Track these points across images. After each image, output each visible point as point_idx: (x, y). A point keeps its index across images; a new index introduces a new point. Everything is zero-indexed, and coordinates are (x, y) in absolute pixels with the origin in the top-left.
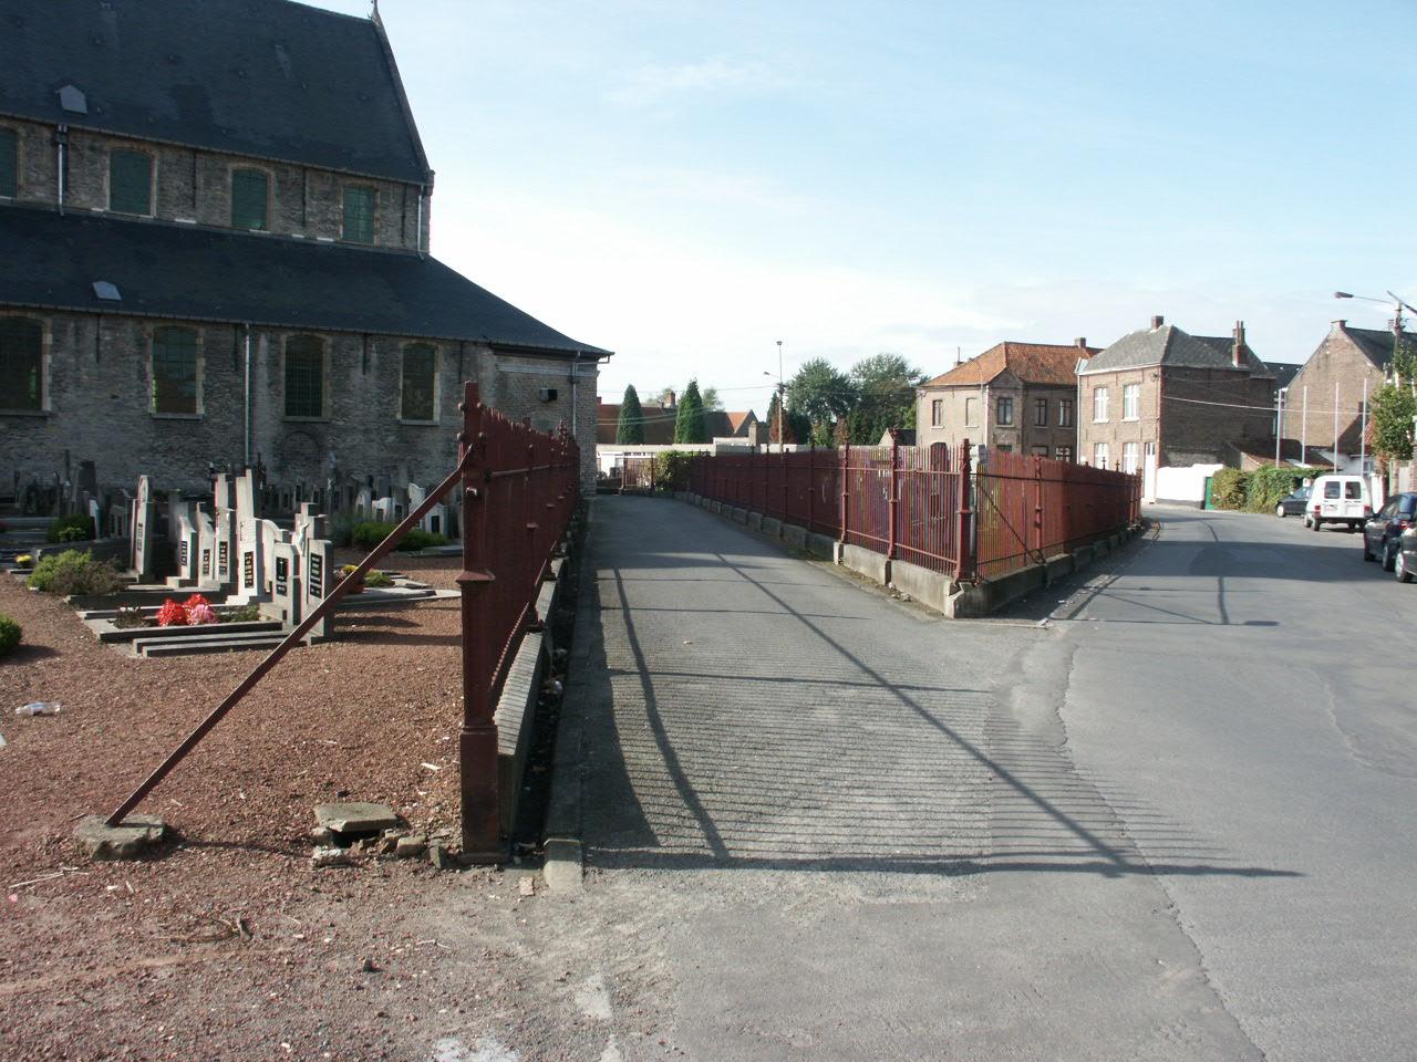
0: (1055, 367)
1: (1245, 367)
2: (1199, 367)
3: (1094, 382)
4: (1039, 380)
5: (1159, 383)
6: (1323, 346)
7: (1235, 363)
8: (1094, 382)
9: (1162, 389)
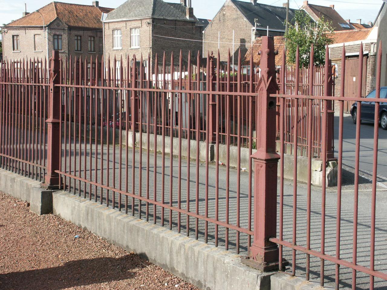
0: (84, 17)
1: (192, 19)
2: (171, 19)
3: (112, 26)
4: (76, 25)
5: (151, 27)
6: (222, 9)
7: (188, 17)
8: (112, 26)
9: (152, 31)
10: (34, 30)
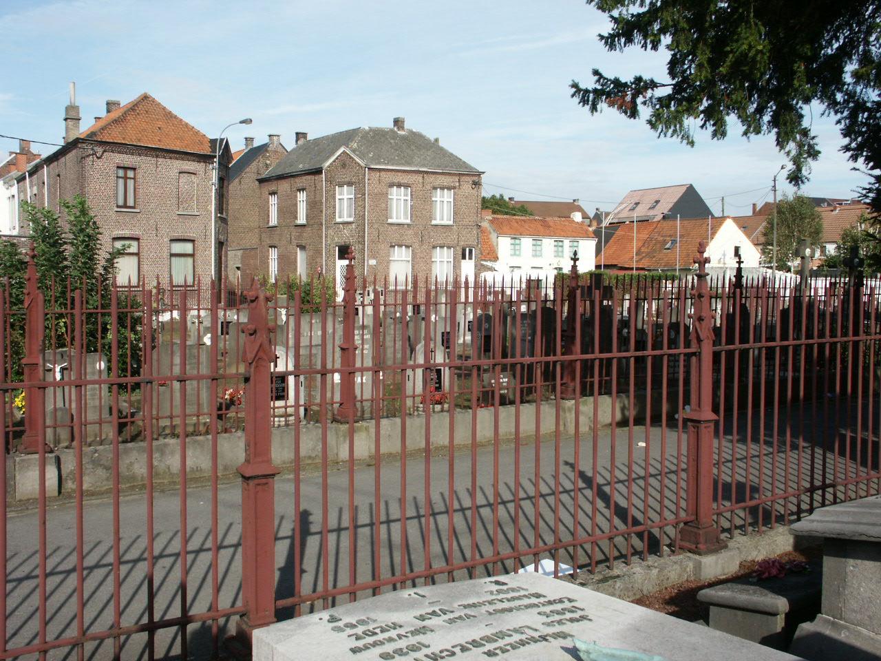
10: (181, 162)
